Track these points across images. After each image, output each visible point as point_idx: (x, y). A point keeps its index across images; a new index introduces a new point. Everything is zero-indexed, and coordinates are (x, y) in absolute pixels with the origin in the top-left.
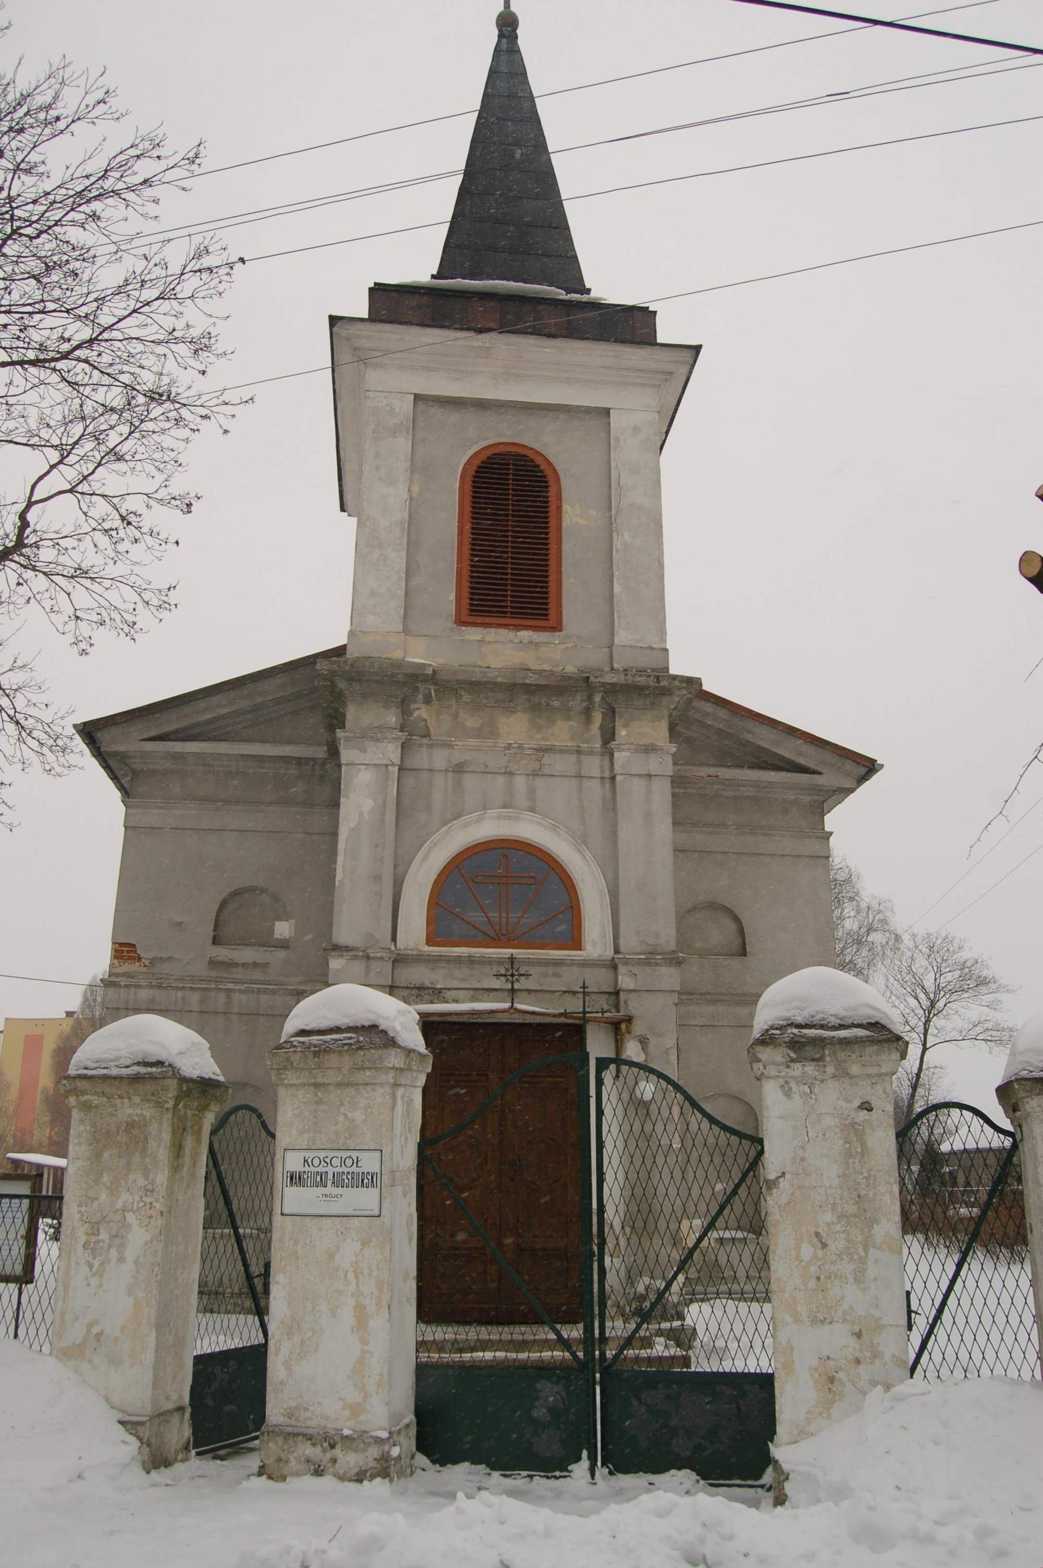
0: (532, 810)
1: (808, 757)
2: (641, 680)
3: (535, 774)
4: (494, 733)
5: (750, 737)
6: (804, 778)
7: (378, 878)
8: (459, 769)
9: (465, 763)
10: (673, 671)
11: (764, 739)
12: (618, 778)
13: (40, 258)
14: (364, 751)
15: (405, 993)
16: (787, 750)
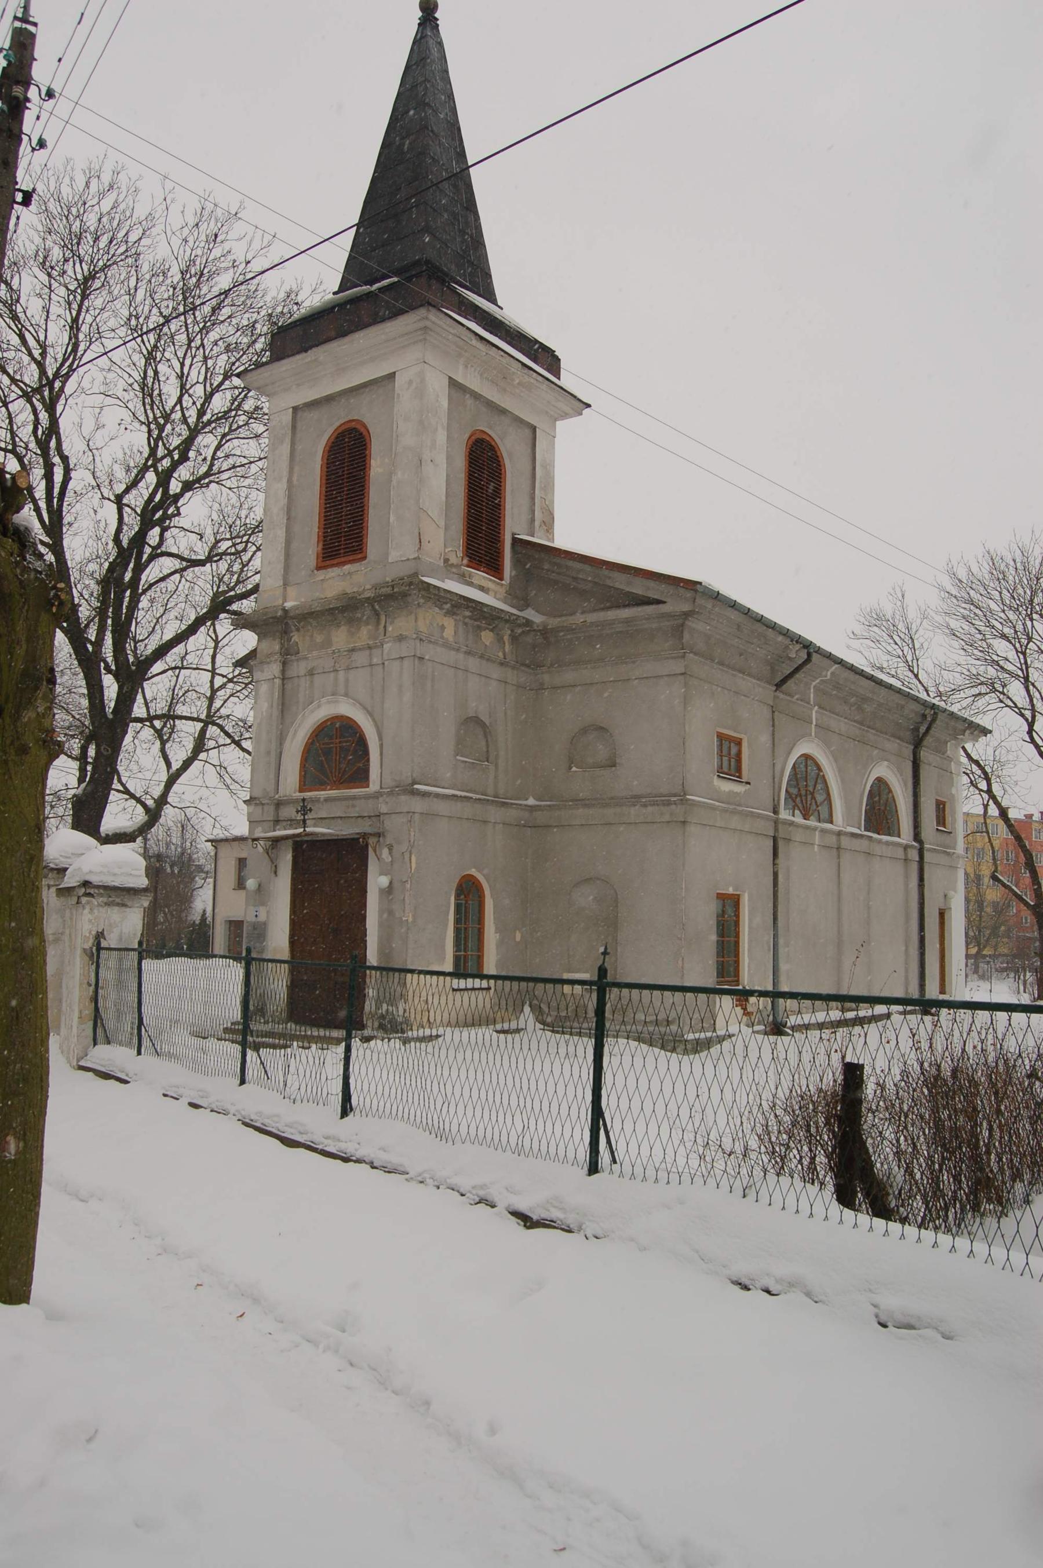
0: (346, 695)
1: (654, 591)
2: (384, 591)
3: (348, 669)
4: (328, 643)
5: (609, 583)
6: (650, 609)
7: (269, 753)
8: (311, 673)
9: (313, 669)
10: (567, 536)
11: (620, 582)
12: (386, 663)
13: (180, 401)
14: (262, 671)
15: (284, 824)
16: (638, 588)
